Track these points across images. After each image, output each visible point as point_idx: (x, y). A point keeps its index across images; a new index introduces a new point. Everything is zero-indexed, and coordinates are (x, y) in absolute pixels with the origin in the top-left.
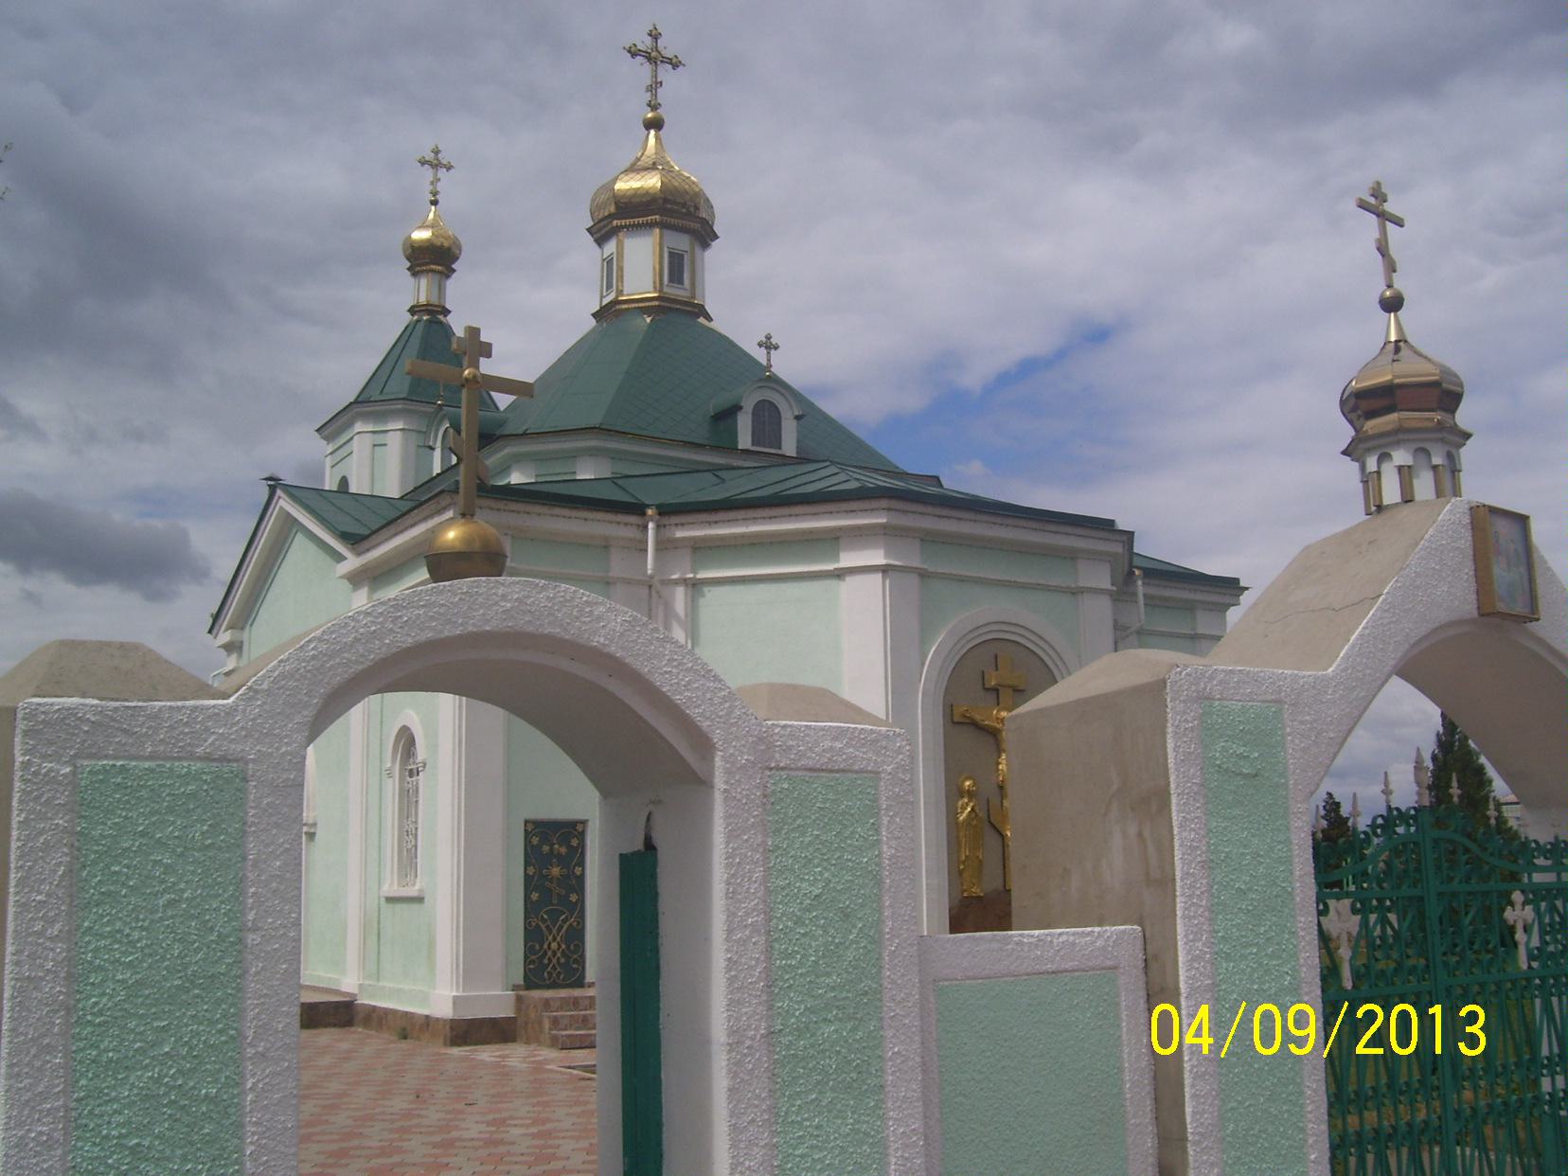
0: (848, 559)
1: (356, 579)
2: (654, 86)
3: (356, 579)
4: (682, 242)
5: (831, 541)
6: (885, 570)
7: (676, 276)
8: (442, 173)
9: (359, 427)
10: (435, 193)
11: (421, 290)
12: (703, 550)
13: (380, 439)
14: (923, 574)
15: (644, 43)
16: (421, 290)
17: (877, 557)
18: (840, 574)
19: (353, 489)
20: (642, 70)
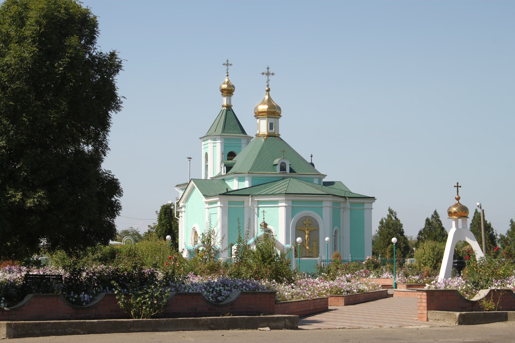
0: (280, 204)
1: (206, 203)
2: (268, 80)
3: (206, 203)
4: (272, 120)
5: (276, 202)
6: (285, 206)
7: (271, 128)
8: (229, 67)
9: (209, 141)
10: (227, 73)
11: (225, 101)
12: (259, 202)
13: (215, 145)
14: (209, 208)
15: (266, 71)
16: (225, 101)
17: (284, 204)
18: (279, 207)
19: (142, 233)
20: (265, 77)
